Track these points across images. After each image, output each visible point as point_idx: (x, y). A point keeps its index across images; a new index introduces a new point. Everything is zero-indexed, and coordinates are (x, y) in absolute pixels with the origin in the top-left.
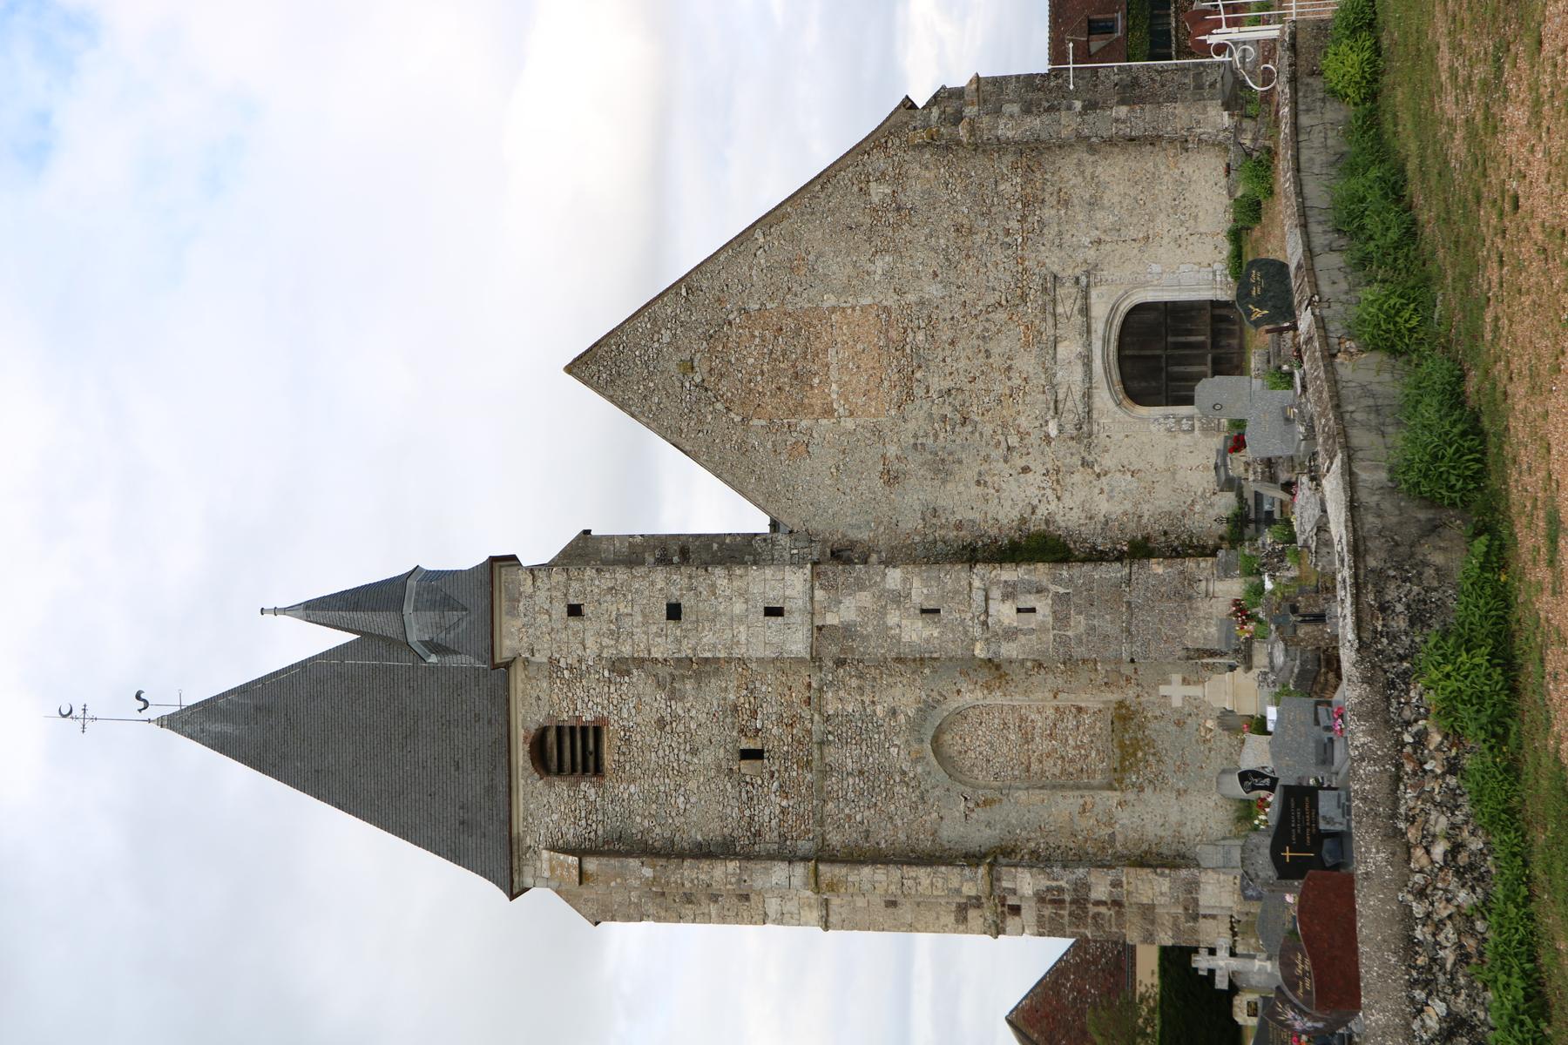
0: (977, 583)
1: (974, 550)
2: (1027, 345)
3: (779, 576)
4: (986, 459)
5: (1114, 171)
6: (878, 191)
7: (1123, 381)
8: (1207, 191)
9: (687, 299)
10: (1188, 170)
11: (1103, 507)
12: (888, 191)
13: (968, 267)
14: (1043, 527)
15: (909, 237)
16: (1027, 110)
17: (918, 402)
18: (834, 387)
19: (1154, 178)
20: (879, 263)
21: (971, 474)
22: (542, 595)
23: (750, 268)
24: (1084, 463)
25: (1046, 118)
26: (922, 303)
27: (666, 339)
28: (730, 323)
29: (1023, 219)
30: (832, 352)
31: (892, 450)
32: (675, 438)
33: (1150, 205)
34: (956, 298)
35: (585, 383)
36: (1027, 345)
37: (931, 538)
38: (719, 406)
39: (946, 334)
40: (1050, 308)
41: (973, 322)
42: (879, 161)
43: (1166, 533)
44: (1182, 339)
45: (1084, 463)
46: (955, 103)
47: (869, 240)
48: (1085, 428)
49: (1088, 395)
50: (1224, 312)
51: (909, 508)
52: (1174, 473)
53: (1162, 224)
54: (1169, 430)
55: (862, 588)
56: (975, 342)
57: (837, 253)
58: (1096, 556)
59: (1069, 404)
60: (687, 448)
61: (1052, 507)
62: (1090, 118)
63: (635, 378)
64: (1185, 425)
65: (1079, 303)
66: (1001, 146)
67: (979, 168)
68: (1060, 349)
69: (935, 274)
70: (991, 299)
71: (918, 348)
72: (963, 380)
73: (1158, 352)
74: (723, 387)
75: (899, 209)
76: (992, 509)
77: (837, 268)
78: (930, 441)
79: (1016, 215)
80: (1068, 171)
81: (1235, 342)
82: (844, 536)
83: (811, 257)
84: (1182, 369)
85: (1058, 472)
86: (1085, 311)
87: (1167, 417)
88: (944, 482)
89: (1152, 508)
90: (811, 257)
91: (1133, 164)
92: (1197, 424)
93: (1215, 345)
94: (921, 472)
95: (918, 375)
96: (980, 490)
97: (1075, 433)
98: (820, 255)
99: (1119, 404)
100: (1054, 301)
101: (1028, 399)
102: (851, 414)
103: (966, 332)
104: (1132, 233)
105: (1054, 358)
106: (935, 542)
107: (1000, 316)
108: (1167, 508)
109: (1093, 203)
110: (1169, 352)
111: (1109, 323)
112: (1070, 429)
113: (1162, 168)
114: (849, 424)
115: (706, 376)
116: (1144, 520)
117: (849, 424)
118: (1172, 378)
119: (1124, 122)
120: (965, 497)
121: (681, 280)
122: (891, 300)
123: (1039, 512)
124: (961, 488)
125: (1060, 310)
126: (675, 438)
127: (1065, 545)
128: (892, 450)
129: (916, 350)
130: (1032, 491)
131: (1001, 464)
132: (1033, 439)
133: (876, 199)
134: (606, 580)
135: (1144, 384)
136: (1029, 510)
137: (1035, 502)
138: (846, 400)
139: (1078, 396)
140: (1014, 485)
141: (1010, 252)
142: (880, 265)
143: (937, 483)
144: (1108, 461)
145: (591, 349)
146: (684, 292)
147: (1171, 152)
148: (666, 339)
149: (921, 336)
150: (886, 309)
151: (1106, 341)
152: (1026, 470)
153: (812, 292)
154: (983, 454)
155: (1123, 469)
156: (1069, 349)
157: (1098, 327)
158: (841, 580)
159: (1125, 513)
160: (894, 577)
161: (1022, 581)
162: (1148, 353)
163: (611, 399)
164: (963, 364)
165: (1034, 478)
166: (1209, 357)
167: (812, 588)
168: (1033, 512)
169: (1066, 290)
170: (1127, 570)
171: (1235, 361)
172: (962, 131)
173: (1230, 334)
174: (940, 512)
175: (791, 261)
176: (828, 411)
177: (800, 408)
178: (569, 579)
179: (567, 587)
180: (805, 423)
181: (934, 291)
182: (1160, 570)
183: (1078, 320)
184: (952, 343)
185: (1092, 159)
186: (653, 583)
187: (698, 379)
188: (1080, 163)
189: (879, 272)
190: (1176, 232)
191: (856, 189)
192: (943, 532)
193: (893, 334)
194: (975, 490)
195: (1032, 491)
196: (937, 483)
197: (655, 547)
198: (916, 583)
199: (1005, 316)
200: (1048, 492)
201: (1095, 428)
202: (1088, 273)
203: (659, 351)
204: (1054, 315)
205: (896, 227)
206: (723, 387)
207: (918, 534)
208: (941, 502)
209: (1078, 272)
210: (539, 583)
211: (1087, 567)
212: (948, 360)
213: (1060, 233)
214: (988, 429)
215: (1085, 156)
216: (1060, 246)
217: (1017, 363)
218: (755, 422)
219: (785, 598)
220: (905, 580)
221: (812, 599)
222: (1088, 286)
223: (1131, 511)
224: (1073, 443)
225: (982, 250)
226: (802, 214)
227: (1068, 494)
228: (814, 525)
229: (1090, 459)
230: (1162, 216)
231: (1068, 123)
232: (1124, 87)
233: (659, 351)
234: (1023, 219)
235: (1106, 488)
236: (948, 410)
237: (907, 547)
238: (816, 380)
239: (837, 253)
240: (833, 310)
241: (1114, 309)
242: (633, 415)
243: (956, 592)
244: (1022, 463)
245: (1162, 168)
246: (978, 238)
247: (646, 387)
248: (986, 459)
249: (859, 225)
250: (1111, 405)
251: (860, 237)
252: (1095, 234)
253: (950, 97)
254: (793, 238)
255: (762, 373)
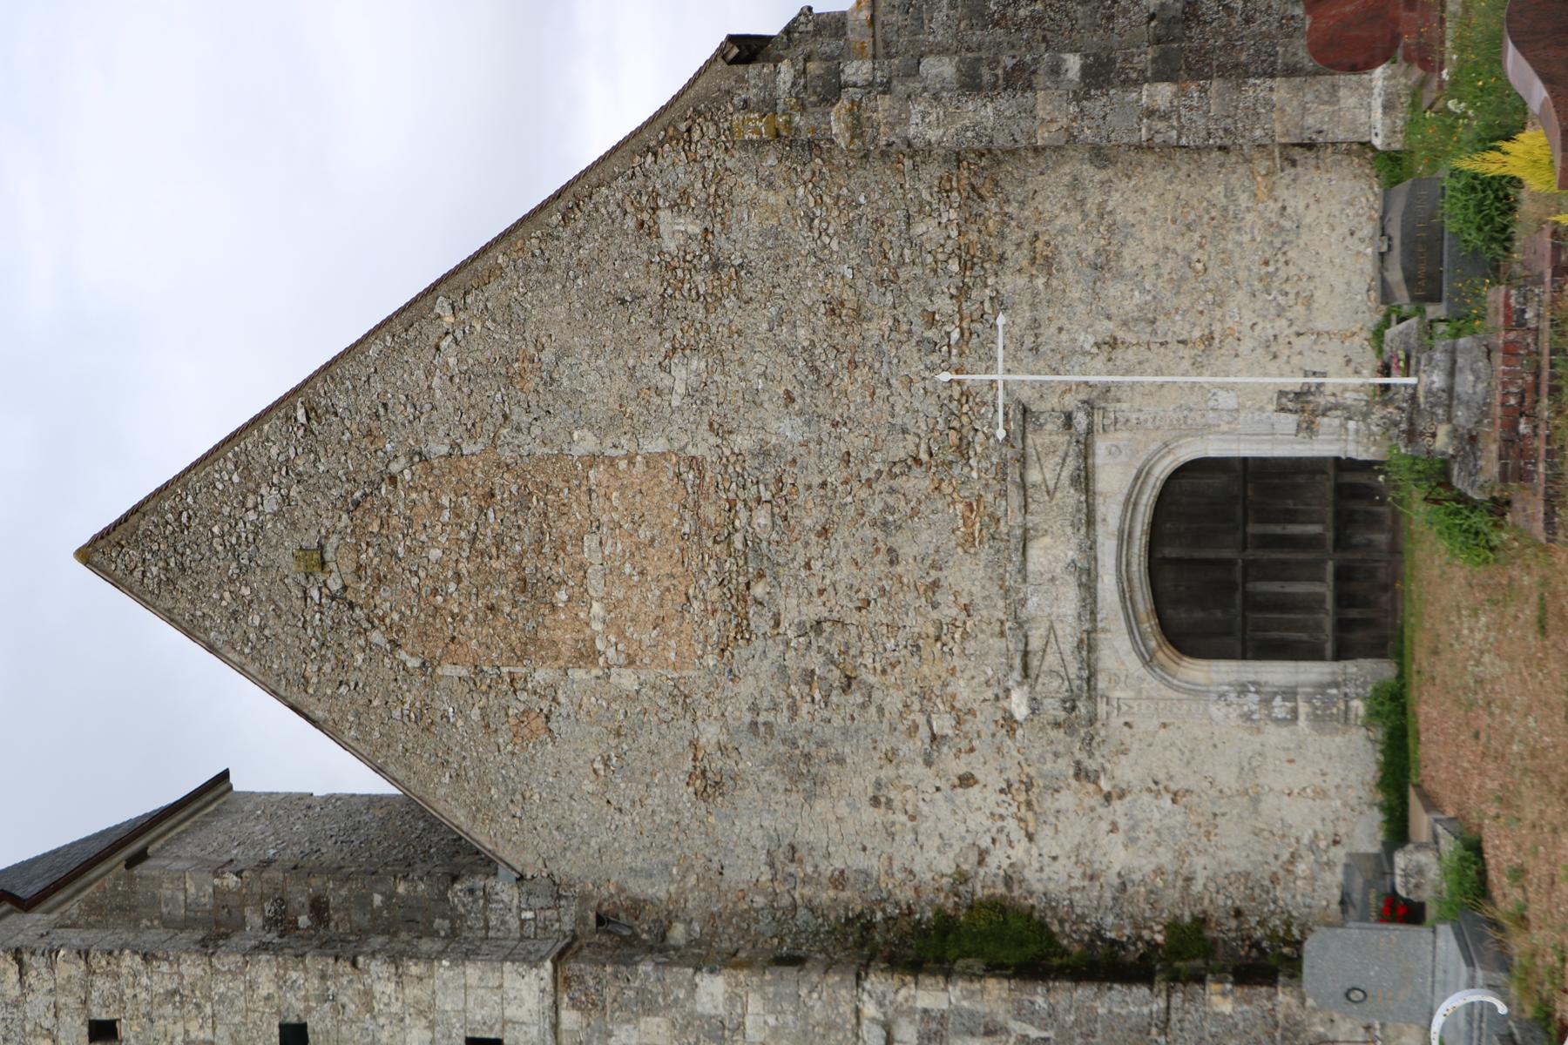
0: (870, 1009)
1: (869, 926)
2: (969, 541)
3: (493, 980)
4: (891, 757)
5: (1144, 204)
6: (676, 229)
7: (1159, 611)
8: (1334, 238)
9: (308, 431)
10: (1297, 202)
11: (1117, 857)
12: (695, 229)
13: (852, 385)
14: (1001, 890)
15: (738, 324)
16: (970, 84)
17: (758, 644)
18: (597, 608)
19: (1227, 218)
20: (680, 373)
21: (861, 786)
22: (37, 1004)
23: (429, 374)
24: (1080, 773)
25: (1007, 104)
26: (763, 453)
27: (270, 506)
28: (393, 480)
29: (963, 292)
30: (590, 542)
31: (710, 733)
32: (295, 695)
33: (1216, 273)
34: (829, 446)
35: (117, 583)
36: (969, 541)
37: (785, 901)
38: (376, 637)
39: (811, 517)
40: (1013, 472)
41: (864, 493)
42: (674, 170)
43: (1238, 913)
44: (1277, 529)
45: (1080, 773)
46: (828, 46)
47: (659, 326)
48: (1082, 708)
49: (1087, 645)
50: (1361, 478)
51: (742, 844)
52: (1256, 801)
53: (1240, 311)
54: (1247, 717)
55: (650, 1009)
56: (868, 532)
57: (598, 349)
58: (1107, 964)
59: (1052, 660)
60: (319, 714)
61: (1019, 852)
62: (1096, 106)
63: (214, 577)
64: (1280, 708)
65: (1071, 463)
66: (917, 152)
67: (872, 190)
68: (1034, 552)
69: (790, 398)
70: (899, 449)
71: (757, 541)
72: (843, 605)
73: (1227, 554)
74: (384, 600)
75: (716, 266)
76: (903, 851)
77: (597, 379)
78: (782, 719)
79: (947, 286)
80: (1052, 202)
81: (1381, 538)
82: (621, 890)
83: (547, 356)
84: (1274, 587)
85: (1029, 786)
86: (1084, 480)
87: (1242, 689)
88: (810, 797)
89: (1212, 865)
90: (547, 356)
91: (1183, 189)
92: (1303, 708)
93: (1341, 543)
94: (766, 777)
95: (759, 590)
96: (878, 815)
97: (1062, 715)
98: (563, 353)
99: (1148, 661)
100: (1023, 460)
101: (971, 646)
102: (631, 662)
103: (851, 512)
104: (1181, 327)
105: (1023, 569)
106: (795, 907)
107: (918, 483)
108: (1243, 865)
109: (1102, 267)
110: (1251, 554)
111: (1131, 503)
112: (1053, 709)
113: (1244, 199)
114: (627, 680)
115: (349, 580)
116: (1197, 887)
117: (627, 680)
118: (1254, 603)
119: (1165, 117)
120: (849, 827)
121: (296, 391)
122: (703, 446)
123: (992, 861)
124: (842, 810)
125: (1034, 476)
126: (295, 695)
127: (1043, 926)
128: (710, 733)
129: (753, 545)
130: (978, 821)
131: (919, 769)
132: (984, 721)
133: (670, 245)
134: (162, 978)
135: (1198, 615)
136: (973, 857)
137: (985, 842)
138: (621, 634)
139: (1068, 645)
140: (944, 810)
141: (935, 358)
142: (681, 376)
143: (796, 798)
144: (1125, 771)
145: (125, 518)
146: (301, 414)
147: (1262, 166)
148: (270, 506)
149: (762, 518)
150: (694, 463)
151: (1125, 538)
152: (966, 781)
153: (551, 425)
154: (883, 747)
155: (1155, 788)
156: (1052, 552)
157: (1110, 513)
158: (610, 993)
159: (1160, 871)
160: (712, 991)
161: (958, 1012)
162: (1210, 554)
163: (170, 617)
164: (844, 573)
165: (984, 797)
166: (1330, 567)
167: (556, 1007)
168: (981, 862)
169: (1047, 438)
170: (1160, 1003)
171: (1382, 576)
172: (837, 123)
173: (1373, 521)
174: (802, 852)
175: (507, 363)
176: (587, 655)
177: (529, 648)
178: (90, 972)
179: (87, 988)
180: (542, 675)
181: (787, 430)
182: (1226, 1007)
183: (1070, 497)
184: (824, 532)
185: (1100, 176)
186: (252, 986)
187: (335, 585)
188: (1075, 183)
189: (680, 389)
190: (1267, 329)
191: (630, 223)
192: (808, 891)
193: (709, 512)
194: (870, 814)
195: (978, 821)
196: (796, 798)
197: (263, 898)
198: (755, 1004)
199: (926, 484)
200: (1011, 824)
201: (1102, 708)
202: (1089, 406)
203: (259, 528)
204: (1023, 486)
205: (711, 302)
206: (384, 600)
207: (763, 892)
208: (803, 836)
209: (1071, 402)
210: (31, 978)
211: (1084, 992)
212: (817, 565)
213: (1035, 324)
214: (893, 702)
215: (1087, 170)
216: (1035, 349)
217: (950, 577)
218: (447, 670)
219: (505, 1023)
220: (732, 999)
221: (555, 1026)
222: (1090, 430)
223: (1169, 868)
224: (1059, 734)
225: (880, 353)
226: (527, 269)
227: (1048, 831)
228: (566, 867)
229: (1090, 764)
230: (1241, 295)
231: (1050, 112)
232: (1168, 23)
233: (259, 528)
234: (963, 292)
235: (1123, 823)
236: (815, 662)
237: (742, 915)
238: (562, 596)
239: (598, 349)
240: (592, 460)
241: (1141, 476)
242: (211, 648)
243: (830, 1026)
244: (958, 767)
245: (1244, 199)
246: (873, 329)
247: (236, 596)
248: (891, 757)
249: (639, 297)
250: (1134, 664)
251: (640, 318)
252: (1105, 328)
253: (818, 32)
254: (512, 318)
255: (458, 577)
